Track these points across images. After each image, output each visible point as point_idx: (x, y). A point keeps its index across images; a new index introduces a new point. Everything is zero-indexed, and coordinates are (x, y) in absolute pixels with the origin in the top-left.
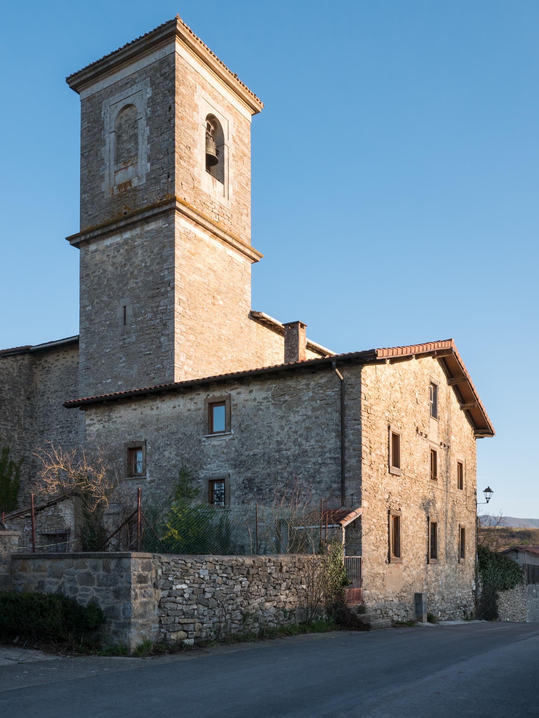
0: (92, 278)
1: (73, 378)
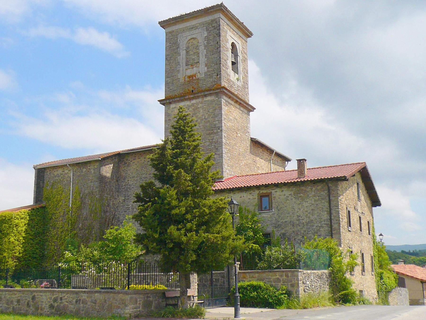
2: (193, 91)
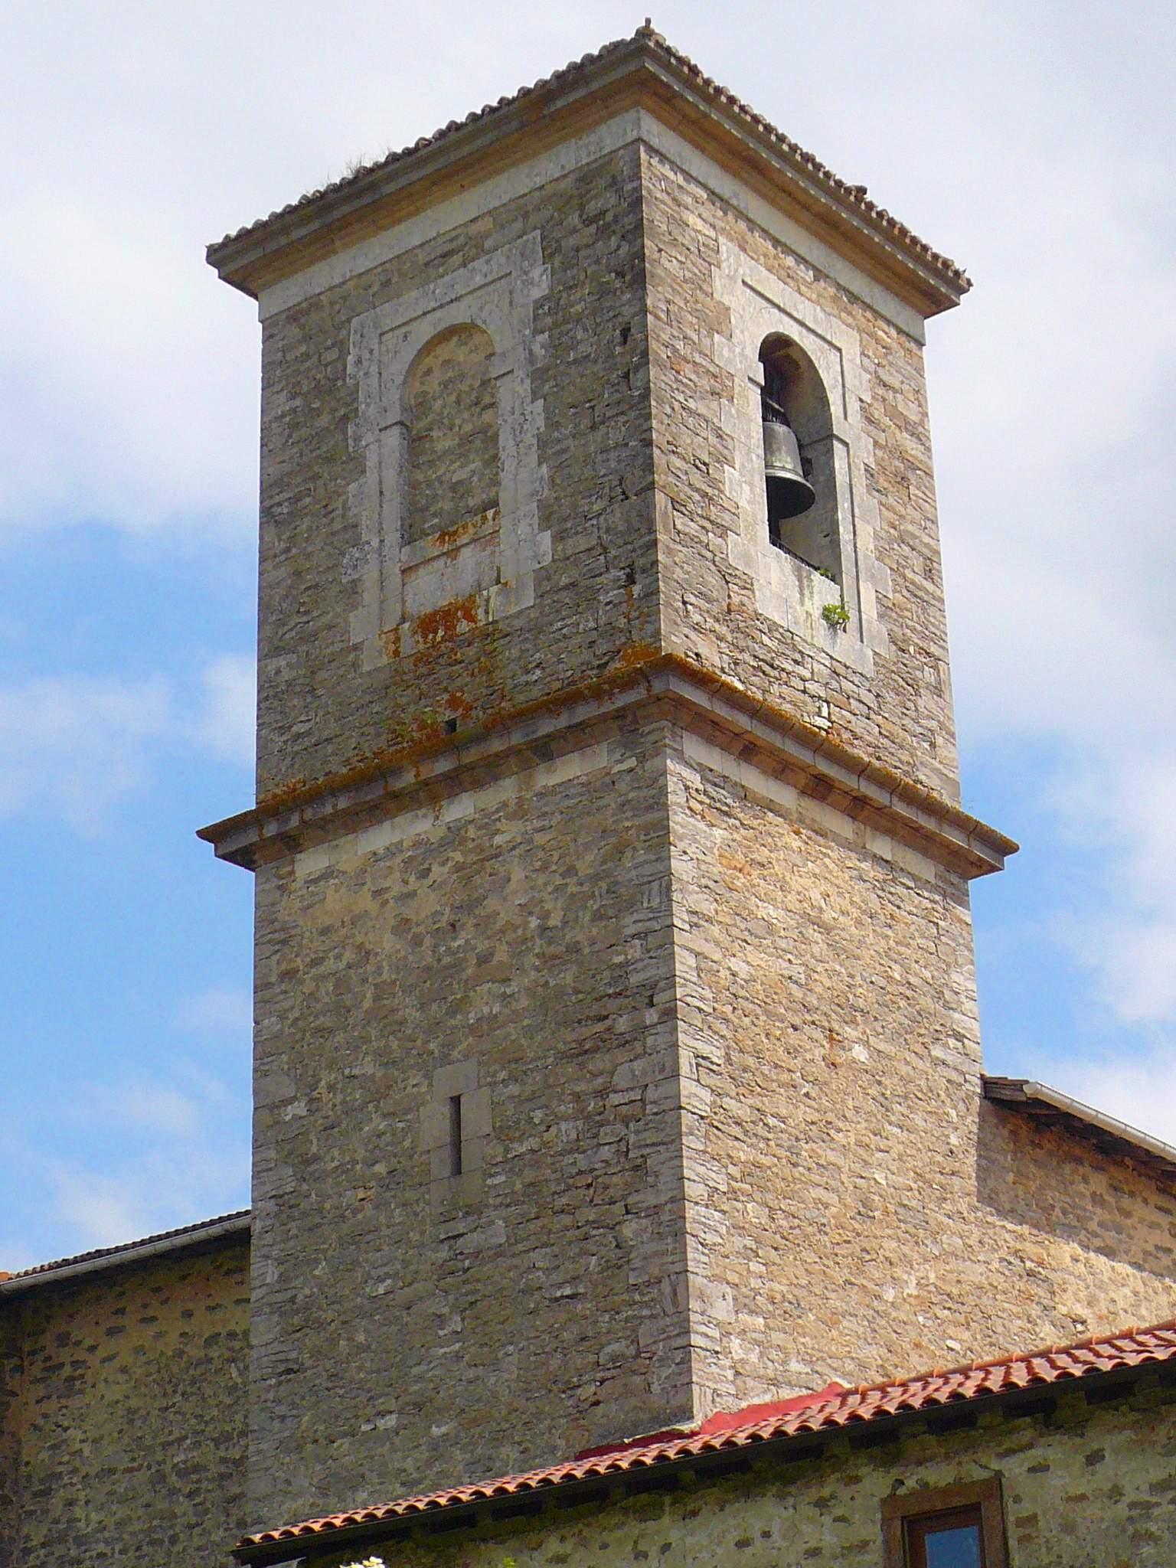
0: (309, 987)
1: (187, 1407)
2: (452, 725)
